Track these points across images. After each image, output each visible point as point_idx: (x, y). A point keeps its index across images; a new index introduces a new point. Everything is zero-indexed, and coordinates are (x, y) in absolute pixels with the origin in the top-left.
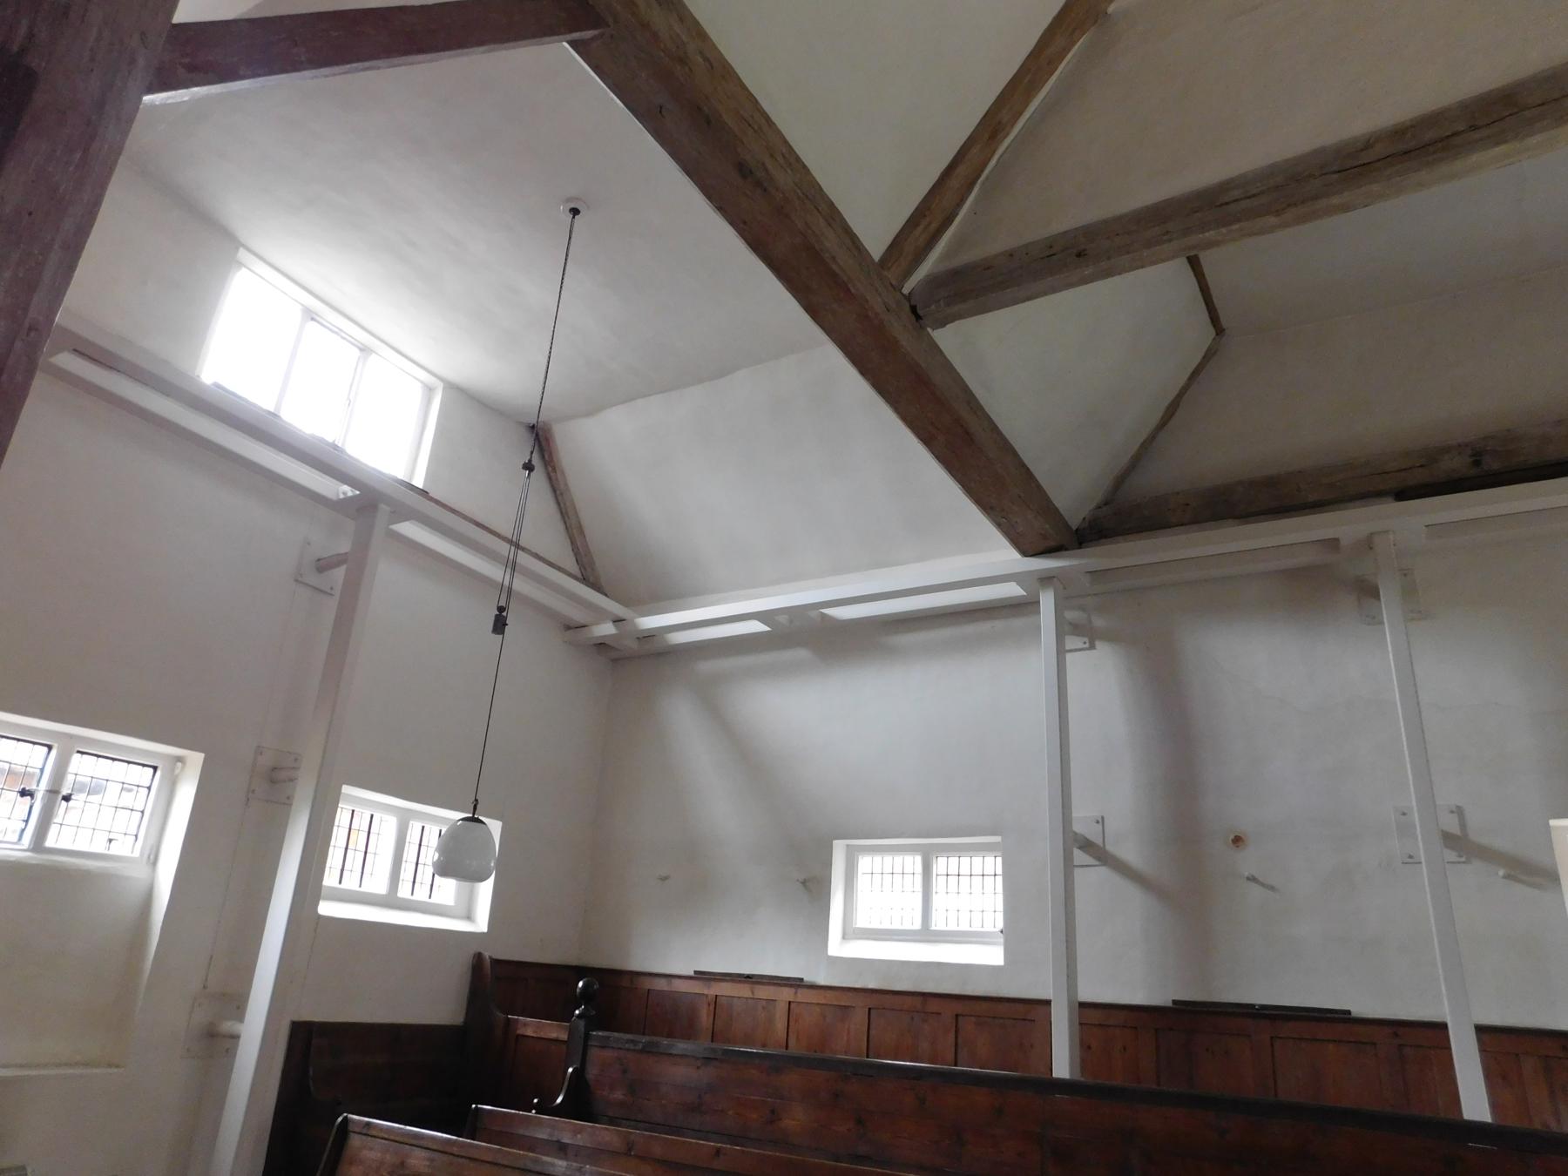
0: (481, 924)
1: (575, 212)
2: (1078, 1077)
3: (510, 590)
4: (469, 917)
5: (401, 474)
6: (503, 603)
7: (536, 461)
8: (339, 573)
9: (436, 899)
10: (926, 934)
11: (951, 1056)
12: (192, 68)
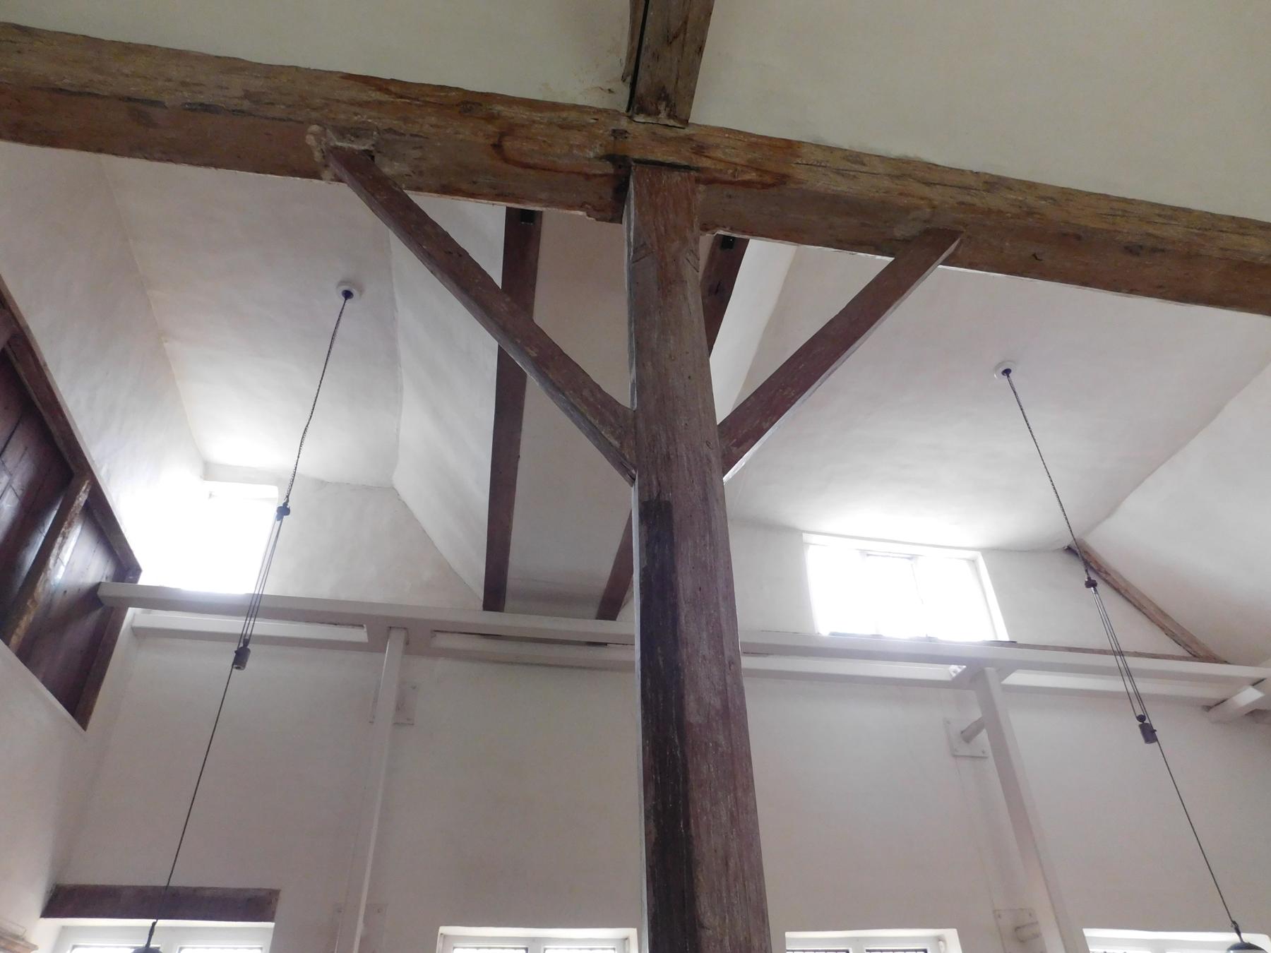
1: (1007, 372)
3: (1138, 695)
5: (990, 637)
6: (1140, 712)
7: (1094, 577)
8: (983, 736)
12: (739, 444)
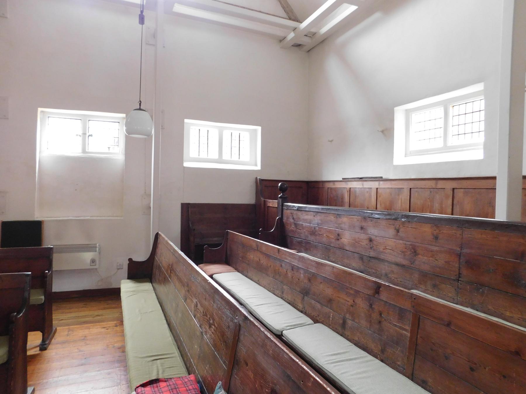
0: (259, 168)
2: (517, 218)
4: (256, 165)
9: (201, 156)
10: (446, 149)
11: (450, 210)
